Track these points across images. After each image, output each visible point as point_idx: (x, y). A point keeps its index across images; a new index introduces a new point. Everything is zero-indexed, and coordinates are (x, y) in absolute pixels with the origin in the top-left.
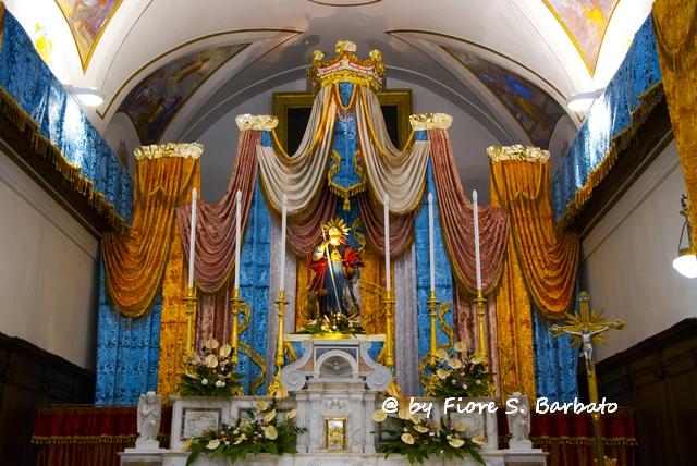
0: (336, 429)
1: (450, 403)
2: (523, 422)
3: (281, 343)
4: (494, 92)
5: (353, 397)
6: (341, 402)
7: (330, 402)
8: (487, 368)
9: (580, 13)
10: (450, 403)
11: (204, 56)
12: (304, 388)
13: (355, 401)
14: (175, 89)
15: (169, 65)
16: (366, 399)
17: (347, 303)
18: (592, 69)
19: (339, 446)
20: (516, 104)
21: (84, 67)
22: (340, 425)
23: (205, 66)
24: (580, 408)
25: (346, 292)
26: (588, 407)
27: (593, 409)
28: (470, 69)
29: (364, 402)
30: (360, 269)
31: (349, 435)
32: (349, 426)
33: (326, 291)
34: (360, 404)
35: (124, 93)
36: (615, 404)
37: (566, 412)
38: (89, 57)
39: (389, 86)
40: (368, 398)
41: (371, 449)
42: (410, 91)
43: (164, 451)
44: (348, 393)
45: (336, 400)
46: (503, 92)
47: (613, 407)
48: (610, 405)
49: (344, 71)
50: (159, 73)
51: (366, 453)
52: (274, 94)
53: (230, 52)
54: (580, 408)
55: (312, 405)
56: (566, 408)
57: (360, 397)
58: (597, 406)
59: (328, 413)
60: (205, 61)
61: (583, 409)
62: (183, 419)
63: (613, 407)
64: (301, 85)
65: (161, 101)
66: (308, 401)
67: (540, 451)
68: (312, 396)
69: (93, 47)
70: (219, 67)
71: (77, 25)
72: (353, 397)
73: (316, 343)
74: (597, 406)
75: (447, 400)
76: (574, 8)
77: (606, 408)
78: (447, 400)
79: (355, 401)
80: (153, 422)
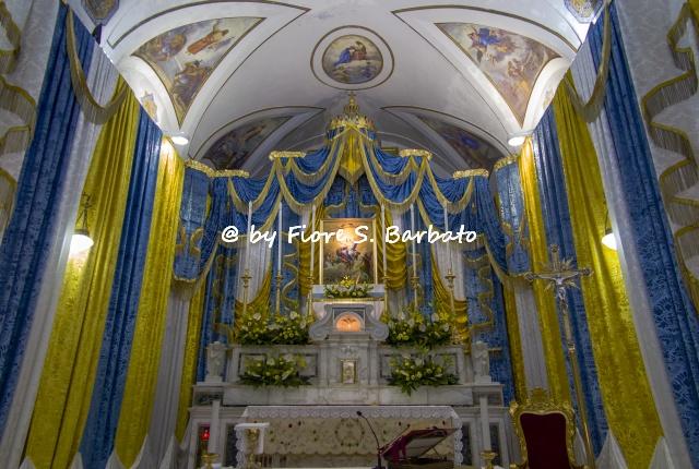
0: (349, 368)
1: (294, 231)
2: (484, 363)
4: (452, 145)
5: (361, 345)
9: (512, 84)
10: (294, 231)
11: (262, 123)
13: (363, 348)
14: (243, 146)
15: (240, 128)
18: (521, 120)
19: (351, 381)
20: (468, 154)
21: (180, 124)
22: (352, 365)
23: (263, 132)
24: (257, 236)
26: (443, 235)
27: (409, 237)
29: (369, 349)
31: (358, 372)
32: (358, 366)
35: (209, 145)
36: (474, 232)
37: (419, 242)
38: (183, 118)
39: (383, 146)
41: (374, 382)
43: (224, 384)
44: (357, 342)
46: (458, 145)
47: (471, 236)
48: (469, 233)
50: (232, 134)
51: (372, 386)
53: (280, 120)
54: (257, 236)
56: (419, 236)
57: (366, 345)
58: (454, 235)
59: (342, 356)
60: (263, 127)
61: (438, 237)
62: (239, 362)
63: (471, 236)
65: (235, 154)
66: (329, 348)
67: (497, 384)
68: (332, 345)
69: (185, 111)
70: (131, 31)
71: (175, 96)
72: (361, 345)
74: (454, 235)
75: (291, 229)
76: (508, 81)
77: (464, 236)
78: (291, 229)
79: (363, 348)
80: (218, 363)
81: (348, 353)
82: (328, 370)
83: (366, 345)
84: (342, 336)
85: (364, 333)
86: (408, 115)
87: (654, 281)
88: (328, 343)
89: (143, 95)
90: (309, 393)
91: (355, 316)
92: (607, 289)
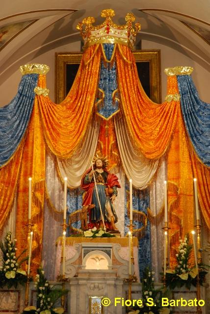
3: (11, 158)
5: (108, 282)
6: (100, 286)
7: (92, 286)
8: (40, 295)
12: (75, 276)
13: (109, 285)
16: (116, 283)
17: (108, 214)
23: (4, 37)
25: (108, 206)
28: (202, 37)
29: (115, 286)
30: (118, 189)
33: (93, 206)
34: (112, 287)
40: (118, 283)
42: (159, 52)
44: (104, 279)
45: (97, 284)
49: (114, 36)
52: (56, 54)
55: (82, 288)
57: (113, 282)
60: (4, 33)
64: (75, 47)
66: (78, 285)
68: (81, 282)
70: (10, 17)
72: (108, 282)
73: (83, 246)
81: (96, 290)
82: (78, 305)
83: (113, 282)
84: (91, 273)
85: (112, 271)
86: (167, 17)
87: (201, 114)
88: (78, 280)
89: (185, 167)
90: (62, 309)
91: (102, 255)
92: (19, 157)
